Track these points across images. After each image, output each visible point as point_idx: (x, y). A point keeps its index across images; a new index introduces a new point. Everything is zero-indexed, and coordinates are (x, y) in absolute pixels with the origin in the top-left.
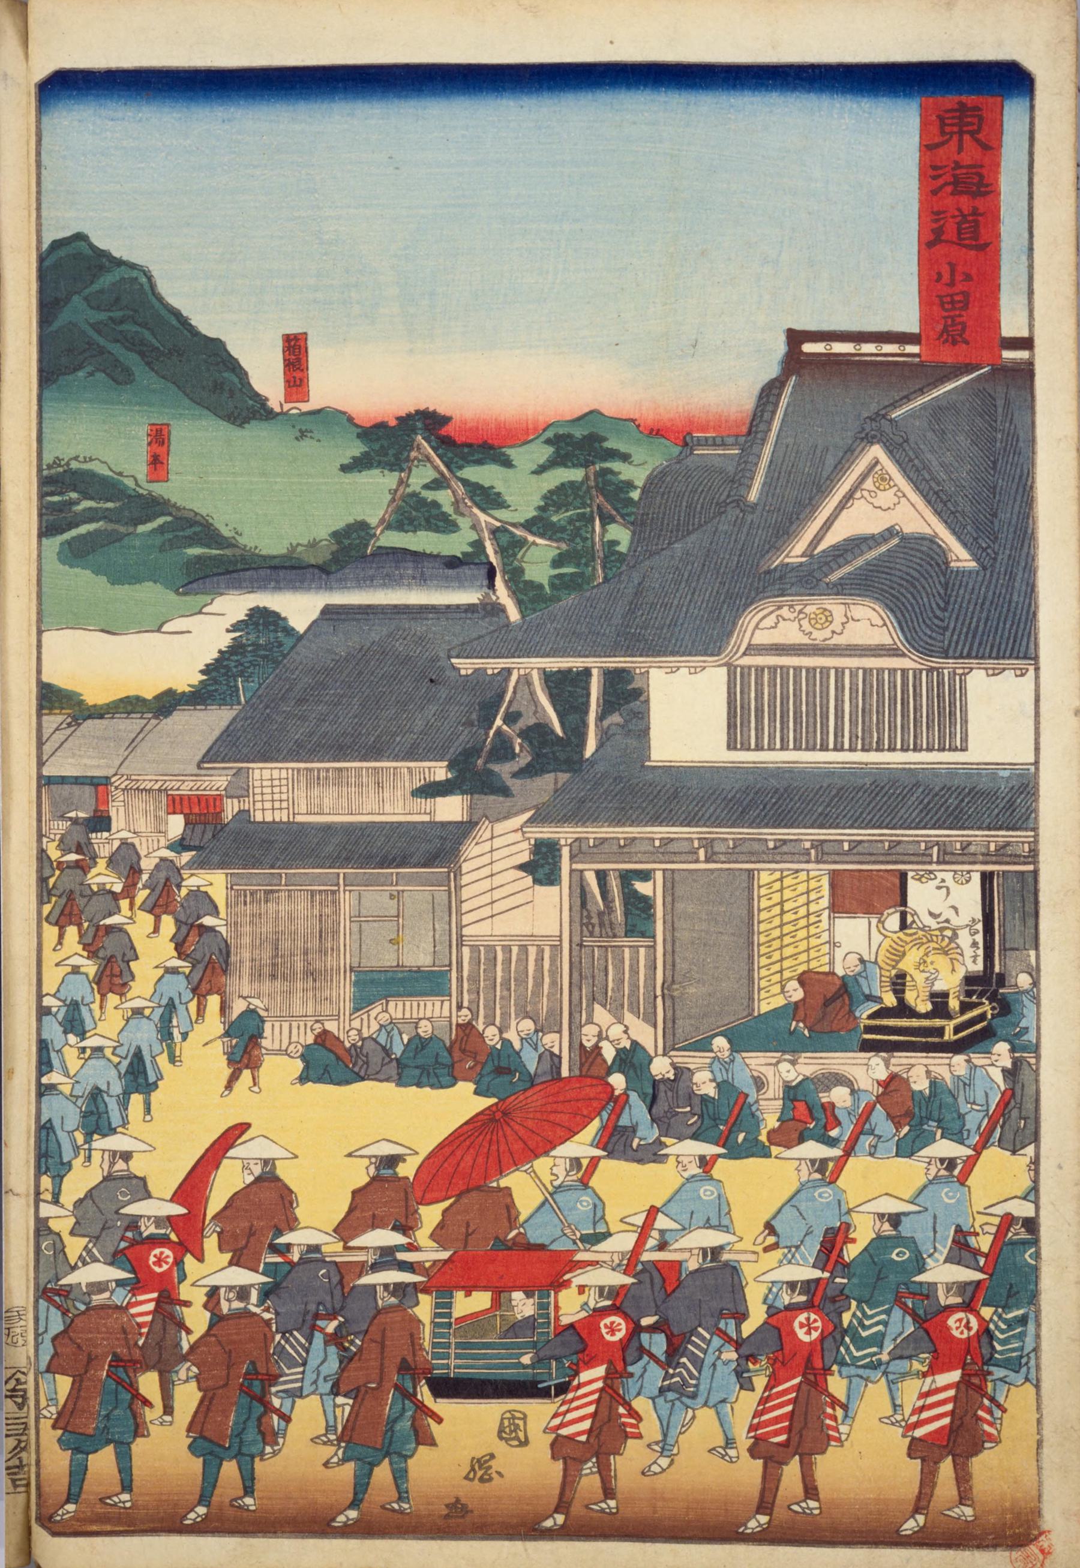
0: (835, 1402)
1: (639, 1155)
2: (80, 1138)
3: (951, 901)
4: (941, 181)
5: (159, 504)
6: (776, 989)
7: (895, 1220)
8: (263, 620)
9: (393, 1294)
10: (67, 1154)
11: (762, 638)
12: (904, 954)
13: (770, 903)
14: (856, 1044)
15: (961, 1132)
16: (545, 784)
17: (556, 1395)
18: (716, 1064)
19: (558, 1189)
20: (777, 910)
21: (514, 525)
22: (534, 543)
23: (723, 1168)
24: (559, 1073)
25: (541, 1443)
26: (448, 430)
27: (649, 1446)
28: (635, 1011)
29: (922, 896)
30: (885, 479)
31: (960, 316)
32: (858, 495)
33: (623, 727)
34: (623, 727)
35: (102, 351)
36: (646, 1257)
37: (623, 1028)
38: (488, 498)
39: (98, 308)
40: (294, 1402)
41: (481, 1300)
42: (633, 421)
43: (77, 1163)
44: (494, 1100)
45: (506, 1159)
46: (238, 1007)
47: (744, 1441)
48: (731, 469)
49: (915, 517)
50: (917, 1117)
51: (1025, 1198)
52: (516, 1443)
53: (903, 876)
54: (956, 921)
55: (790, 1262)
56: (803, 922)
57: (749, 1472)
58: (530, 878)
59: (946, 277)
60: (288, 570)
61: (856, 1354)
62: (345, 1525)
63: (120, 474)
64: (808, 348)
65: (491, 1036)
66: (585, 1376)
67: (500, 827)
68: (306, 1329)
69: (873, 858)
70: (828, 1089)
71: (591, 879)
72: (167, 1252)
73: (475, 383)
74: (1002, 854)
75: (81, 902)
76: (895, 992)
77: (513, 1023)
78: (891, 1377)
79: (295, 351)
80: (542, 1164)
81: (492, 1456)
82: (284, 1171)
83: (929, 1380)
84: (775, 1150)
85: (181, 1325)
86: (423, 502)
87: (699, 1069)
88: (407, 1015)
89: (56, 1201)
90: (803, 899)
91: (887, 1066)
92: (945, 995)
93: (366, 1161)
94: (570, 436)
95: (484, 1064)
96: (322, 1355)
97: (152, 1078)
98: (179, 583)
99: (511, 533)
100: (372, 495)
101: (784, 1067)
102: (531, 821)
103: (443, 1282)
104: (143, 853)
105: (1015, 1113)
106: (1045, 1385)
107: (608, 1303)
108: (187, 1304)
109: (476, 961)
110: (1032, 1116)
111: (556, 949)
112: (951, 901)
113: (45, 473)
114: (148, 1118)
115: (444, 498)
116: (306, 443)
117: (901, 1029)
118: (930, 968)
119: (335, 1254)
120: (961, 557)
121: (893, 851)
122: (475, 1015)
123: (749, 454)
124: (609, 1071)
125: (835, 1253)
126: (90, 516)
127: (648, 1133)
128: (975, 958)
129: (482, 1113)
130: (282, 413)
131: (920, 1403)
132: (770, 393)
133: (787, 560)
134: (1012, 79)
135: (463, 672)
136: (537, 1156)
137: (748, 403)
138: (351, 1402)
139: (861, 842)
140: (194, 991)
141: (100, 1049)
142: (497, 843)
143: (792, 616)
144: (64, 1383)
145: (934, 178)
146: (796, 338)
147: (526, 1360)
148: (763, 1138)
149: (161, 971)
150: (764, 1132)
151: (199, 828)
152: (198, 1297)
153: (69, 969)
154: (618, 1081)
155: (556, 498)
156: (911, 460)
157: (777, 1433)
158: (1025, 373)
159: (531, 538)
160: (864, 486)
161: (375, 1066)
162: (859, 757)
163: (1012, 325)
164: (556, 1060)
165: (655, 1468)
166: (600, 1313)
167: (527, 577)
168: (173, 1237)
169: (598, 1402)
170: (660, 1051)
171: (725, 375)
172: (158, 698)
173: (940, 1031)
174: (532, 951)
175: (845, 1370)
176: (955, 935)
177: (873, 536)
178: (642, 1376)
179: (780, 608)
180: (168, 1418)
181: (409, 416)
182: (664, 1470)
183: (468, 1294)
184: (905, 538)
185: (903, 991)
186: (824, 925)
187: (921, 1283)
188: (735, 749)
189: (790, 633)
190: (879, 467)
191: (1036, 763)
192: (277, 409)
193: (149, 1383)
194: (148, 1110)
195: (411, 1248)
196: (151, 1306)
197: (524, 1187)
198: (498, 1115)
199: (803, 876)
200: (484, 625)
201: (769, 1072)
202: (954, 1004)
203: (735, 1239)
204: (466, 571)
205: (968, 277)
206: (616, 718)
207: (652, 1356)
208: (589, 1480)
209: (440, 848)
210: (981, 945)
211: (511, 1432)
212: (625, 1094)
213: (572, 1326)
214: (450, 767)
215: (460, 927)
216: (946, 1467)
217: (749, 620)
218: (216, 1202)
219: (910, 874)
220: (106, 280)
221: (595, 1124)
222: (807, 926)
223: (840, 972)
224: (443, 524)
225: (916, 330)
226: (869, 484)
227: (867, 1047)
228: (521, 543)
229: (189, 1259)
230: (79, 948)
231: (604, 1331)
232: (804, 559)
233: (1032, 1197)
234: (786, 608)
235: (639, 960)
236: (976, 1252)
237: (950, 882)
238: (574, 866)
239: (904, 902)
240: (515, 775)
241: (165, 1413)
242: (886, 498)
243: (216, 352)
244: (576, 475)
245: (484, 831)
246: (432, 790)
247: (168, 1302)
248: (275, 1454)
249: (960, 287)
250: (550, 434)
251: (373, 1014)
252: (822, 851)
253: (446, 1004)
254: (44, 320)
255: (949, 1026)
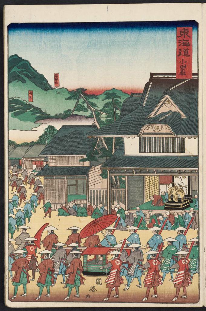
0: (160, 276)
1: (123, 229)
2: (16, 226)
3: (182, 182)
4: (181, 43)
5: (31, 106)
6: (149, 198)
7: (172, 242)
8: (51, 128)
9: (76, 255)
10: (14, 229)
11: (146, 131)
12: (173, 191)
13: (148, 182)
14: (163, 208)
15: (184, 225)
16: (104, 160)
17: (107, 275)
18: (137, 212)
19: (107, 236)
20: (149, 183)
21: (99, 110)
22: (102, 114)
23: (139, 232)
24: (107, 213)
25: (104, 285)
26: (86, 92)
27: (125, 285)
28: (122, 202)
29: (177, 181)
30: (169, 101)
31: (184, 69)
32: (164, 104)
33: (119, 148)
34: (119, 148)
35: (20, 77)
36: (124, 249)
37: (119, 205)
38: (94, 105)
39: (19, 69)
40: (57, 276)
41: (93, 257)
42: (121, 90)
43: (16, 231)
44: (95, 219)
45: (97, 230)
46: (46, 202)
47: (143, 284)
48: (140, 100)
49: (174, 108)
50: (175, 223)
51: (197, 238)
52: (99, 284)
53: (173, 176)
54: (183, 185)
55: (152, 250)
56: (154, 186)
57: (144, 289)
58: (102, 177)
59: (182, 62)
60: (57, 117)
61: (165, 268)
62: (67, 299)
63: (24, 100)
64: (154, 76)
65: (94, 207)
66: (112, 272)
67: (96, 168)
68: (60, 262)
69: (170, 173)
70: (158, 217)
71: (113, 177)
72: (33, 247)
73: (91, 82)
74: (192, 172)
75: (16, 182)
76: (171, 198)
77: (98, 204)
78: (171, 272)
79: (57, 77)
80: (104, 231)
81: (95, 287)
82: (55, 232)
83: (178, 272)
84: (148, 228)
85: (36, 261)
86: (81, 106)
87: (134, 213)
88: (78, 203)
89: (12, 238)
90: (154, 181)
91: (169, 213)
92: (181, 199)
93: (71, 230)
94: (109, 93)
95: (93, 212)
96: (62, 267)
97: (30, 215)
98: (34, 121)
99: (98, 112)
100: (71, 105)
101: (150, 212)
102: (102, 166)
103: (85, 254)
104: (28, 172)
105: (194, 222)
106: (200, 273)
107: (117, 258)
108: (37, 257)
109: (91, 193)
110: (198, 222)
111: (107, 191)
112: (182, 182)
113: (9, 100)
114: (29, 222)
115: (85, 105)
116: (59, 95)
117: (172, 205)
118: (178, 194)
119: (65, 248)
120: (183, 116)
121: (171, 172)
122: (91, 203)
123: (143, 97)
124: (117, 213)
125: (160, 248)
126: (18, 108)
127: (124, 225)
128: (186, 192)
129: (93, 221)
130: (54, 89)
131: (177, 277)
132: (147, 85)
133: (150, 117)
134: (194, 24)
135: (89, 138)
136: (103, 229)
137: (143, 87)
138: (68, 276)
139: (165, 170)
140: (38, 199)
141: (20, 209)
142: (95, 170)
143: (151, 127)
144: (14, 273)
145: (179, 43)
146: (152, 74)
147: (101, 268)
148: (146, 226)
149: (32, 195)
150: (146, 225)
151: (39, 168)
152: (39, 256)
153: (14, 195)
154: (118, 215)
155: (106, 105)
156: (174, 98)
157: (149, 282)
158: (197, 80)
159: (102, 113)
160: (165, 103)
161: (72, 213)
162: (179, 154)
163: (194, 71)
164: (107, 212)
165: (126, 289)
166: (115, 260)
167: (101, 120)
168: (35, 244)
169: (115, 276)
170: (126, 210)
171: (138, 80)
172: (31, 143)
173: (180, 206)
174: (102, 191)
175: (162, 271)
176: (183, 188)
177: (167, 112)
178: (123, 272)
179: (149, 126)
180: (33, 279)
181: (79, 89)
182: (127, 289)
183: (90, 256)
184: (173, 113)
185: (173, 198)
186: (158, 186)
187: (177, 254)
188: (141, 152)
189: (151, 131)
190: (168, 99)
191: (198, 155)
192: (53, 88)
193: (30, 272)
194: (29, 221)
195: (80, 246)
196: (30, 257)
197: (101, 235)
198: (96, 222)
199: (154, 177)
200: (92, 129)
201: (147, 213)
202: (182, 201)
203: (140, 245)
204: (90, 119)
205: (186, 62)
206: (118, 147)
207: (125, 268)
208: (114, 292)
209: (84, 172)
210: (188, 190)
211: (98, 282)
212: (120, 217)
213: (110, 262)
214: (86, 156)
215: (88, 186)
216: (182, 289)
217: (143, 128)
218: (42, 238)
219: (174, 176)
220: (21, 63)
221: (114, 223)
222: (155, 186)
223: (161, 195)
224: (86, 110)
225: (175, 73)
226: (166, 102)
227: (165, 209)
228: (100, 114)
229: (38, 249)
230: (16, 191)
231: (116, 263)
232: (153, 117)
233: (198, 238)
234: (150, 126)
235: (121, 192)
236: (187, 248)
237: (182, 178)
238: (110, 175)
239: (173, 181)
240: (99, 157)
241: (33, 278)
242: (169, 105)
243: (42, 78)
244: (110, 100)
245: (93, 168)
246: (83, 160)
247: (34, 257)
248: (54, 285)
249: (184, 64)
250: (105, 92)
251: (72, 203)
252: (157, 172)
253: (86, 201)
254: (8, 72)
255: (181, 205)
